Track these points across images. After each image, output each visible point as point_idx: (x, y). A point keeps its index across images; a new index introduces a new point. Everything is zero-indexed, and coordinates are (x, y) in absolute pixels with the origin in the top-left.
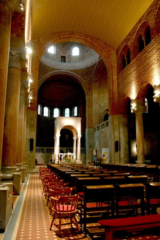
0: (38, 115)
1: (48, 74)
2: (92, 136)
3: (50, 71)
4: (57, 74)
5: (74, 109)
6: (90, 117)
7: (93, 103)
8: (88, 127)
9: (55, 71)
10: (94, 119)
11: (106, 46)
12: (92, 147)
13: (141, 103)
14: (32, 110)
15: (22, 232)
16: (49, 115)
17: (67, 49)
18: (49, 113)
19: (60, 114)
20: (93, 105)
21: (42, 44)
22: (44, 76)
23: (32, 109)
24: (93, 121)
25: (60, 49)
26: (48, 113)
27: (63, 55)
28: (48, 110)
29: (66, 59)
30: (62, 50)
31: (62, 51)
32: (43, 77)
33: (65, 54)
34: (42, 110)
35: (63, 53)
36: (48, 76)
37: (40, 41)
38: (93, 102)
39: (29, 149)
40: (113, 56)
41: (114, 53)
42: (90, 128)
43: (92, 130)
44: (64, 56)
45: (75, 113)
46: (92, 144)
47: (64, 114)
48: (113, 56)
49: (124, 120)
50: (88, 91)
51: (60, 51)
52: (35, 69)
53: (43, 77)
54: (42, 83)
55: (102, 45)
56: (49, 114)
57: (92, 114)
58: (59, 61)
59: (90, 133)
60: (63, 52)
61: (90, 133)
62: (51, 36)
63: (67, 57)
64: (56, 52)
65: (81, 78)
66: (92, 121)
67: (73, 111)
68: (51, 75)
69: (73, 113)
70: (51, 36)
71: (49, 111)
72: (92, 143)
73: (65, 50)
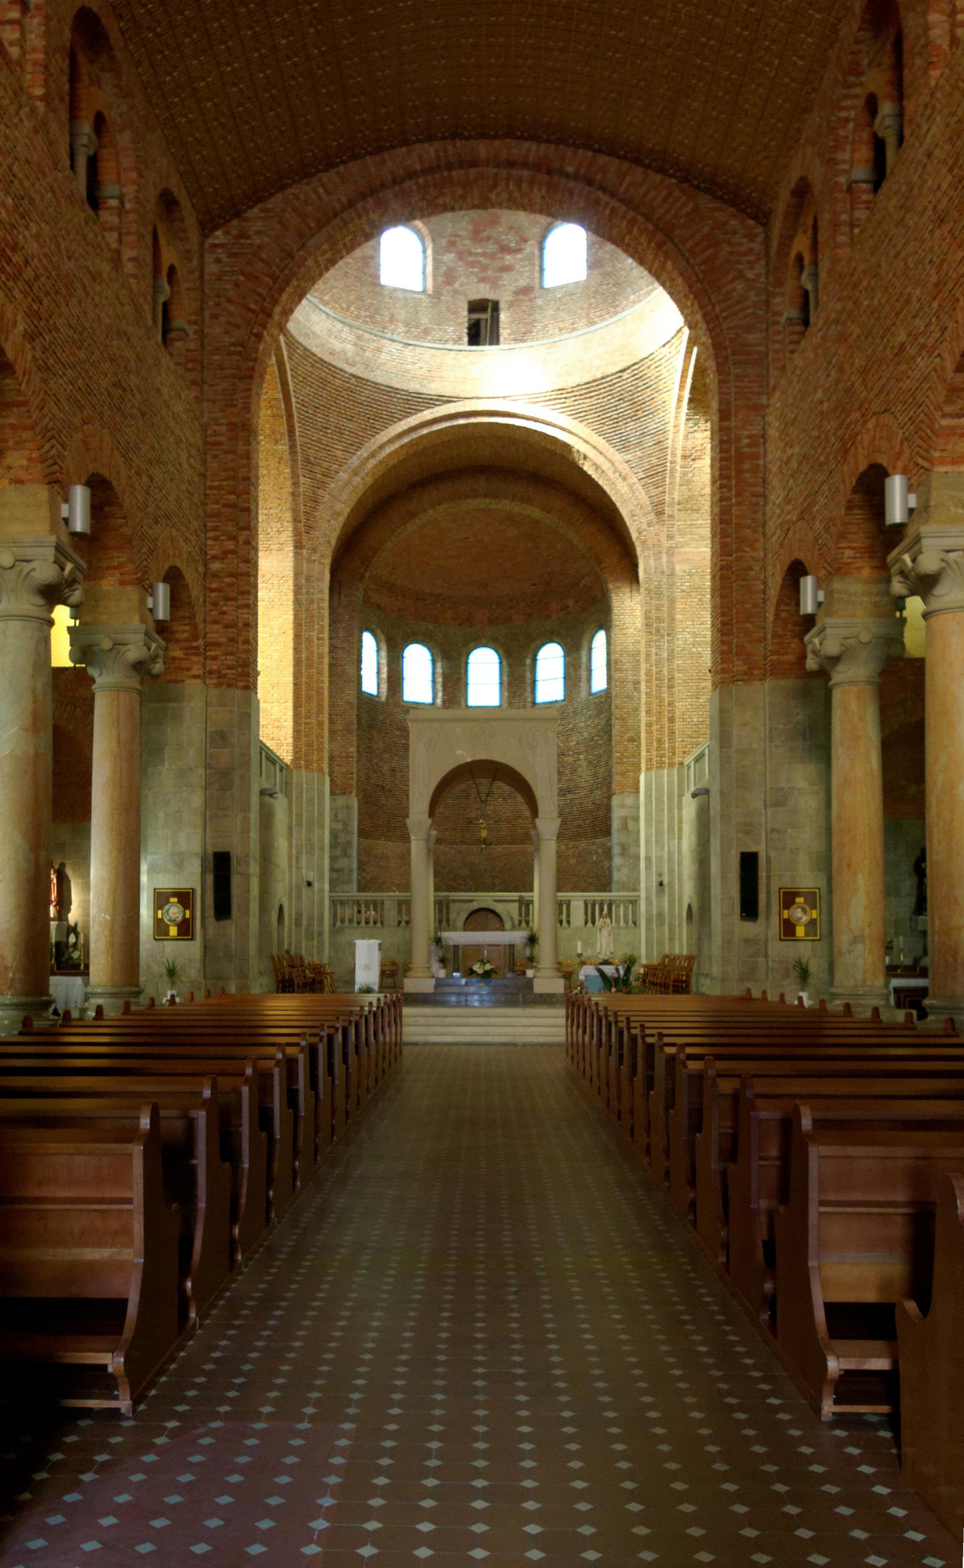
0: (363, 698)
1: (384, 436)
2: (671, 818)
3: (394, 418)
4: (422, 437)
5: (590, 649)
6: (661, 700)
7: (679, 606)
8: (649, 760)
9: (428, 415)
10: (680, 707)
11: (690, 206)
12: (671, 884)
13: (867, 599)
14: (220, 685)
15: (331, 1341)
16: (440, 694)
17: (505, 249)
18: (440, 680)
19: (510, 683)
20: (678, 617)
21: (264, 255)
22: (363, 453)
23: (221, 676)
24: (678, 725)
25: (460, 255)
26: (434, 682)
27: (483, 292)
28: (434, 662)
29: (503, 316)
30: (471, 259)
31: (472, 264)
32: (354, 461)
33: (495, 285)
34: (389, 665)
35: (482, 280)
36: (388, 450)
37: (249, 237)
38: (678, 595)
39: (737, 909)
40: (741, 275)
41: (751, 251)
42: (660, 766)
43: (670, 782)
44: (491, 296)
45: (594, 673)
46: (671, 870)
47: (529, 681)
48: (741, 275)
49: (800, 717)
50: (650, 524)
51: (461, 268)
52: (224, 428)
53: (354, 461)
54: (355, 498)
55: (665, 200)
56: (439, 687)
57: (671, 679)
58: (457, 341)
59: (659, 799)
60: (484, 268)
61: (659, 799)
62: (315, 191)
63: (511, 304)
64: (435, 276)
65: (601, 442)
66: (672, 720)
67: (584, 658)
68: (406, 440)
69: (584, 674)
70: (315, 191)
71: (439, 670)
72: (670, 860)
73: (493, 256)
